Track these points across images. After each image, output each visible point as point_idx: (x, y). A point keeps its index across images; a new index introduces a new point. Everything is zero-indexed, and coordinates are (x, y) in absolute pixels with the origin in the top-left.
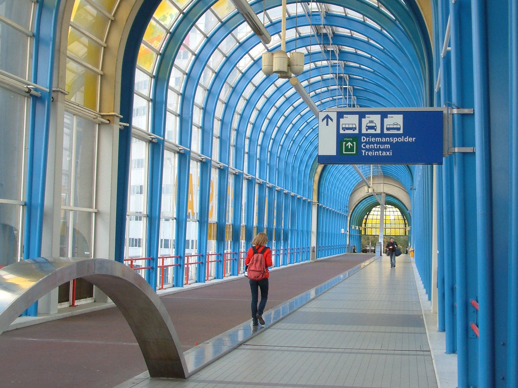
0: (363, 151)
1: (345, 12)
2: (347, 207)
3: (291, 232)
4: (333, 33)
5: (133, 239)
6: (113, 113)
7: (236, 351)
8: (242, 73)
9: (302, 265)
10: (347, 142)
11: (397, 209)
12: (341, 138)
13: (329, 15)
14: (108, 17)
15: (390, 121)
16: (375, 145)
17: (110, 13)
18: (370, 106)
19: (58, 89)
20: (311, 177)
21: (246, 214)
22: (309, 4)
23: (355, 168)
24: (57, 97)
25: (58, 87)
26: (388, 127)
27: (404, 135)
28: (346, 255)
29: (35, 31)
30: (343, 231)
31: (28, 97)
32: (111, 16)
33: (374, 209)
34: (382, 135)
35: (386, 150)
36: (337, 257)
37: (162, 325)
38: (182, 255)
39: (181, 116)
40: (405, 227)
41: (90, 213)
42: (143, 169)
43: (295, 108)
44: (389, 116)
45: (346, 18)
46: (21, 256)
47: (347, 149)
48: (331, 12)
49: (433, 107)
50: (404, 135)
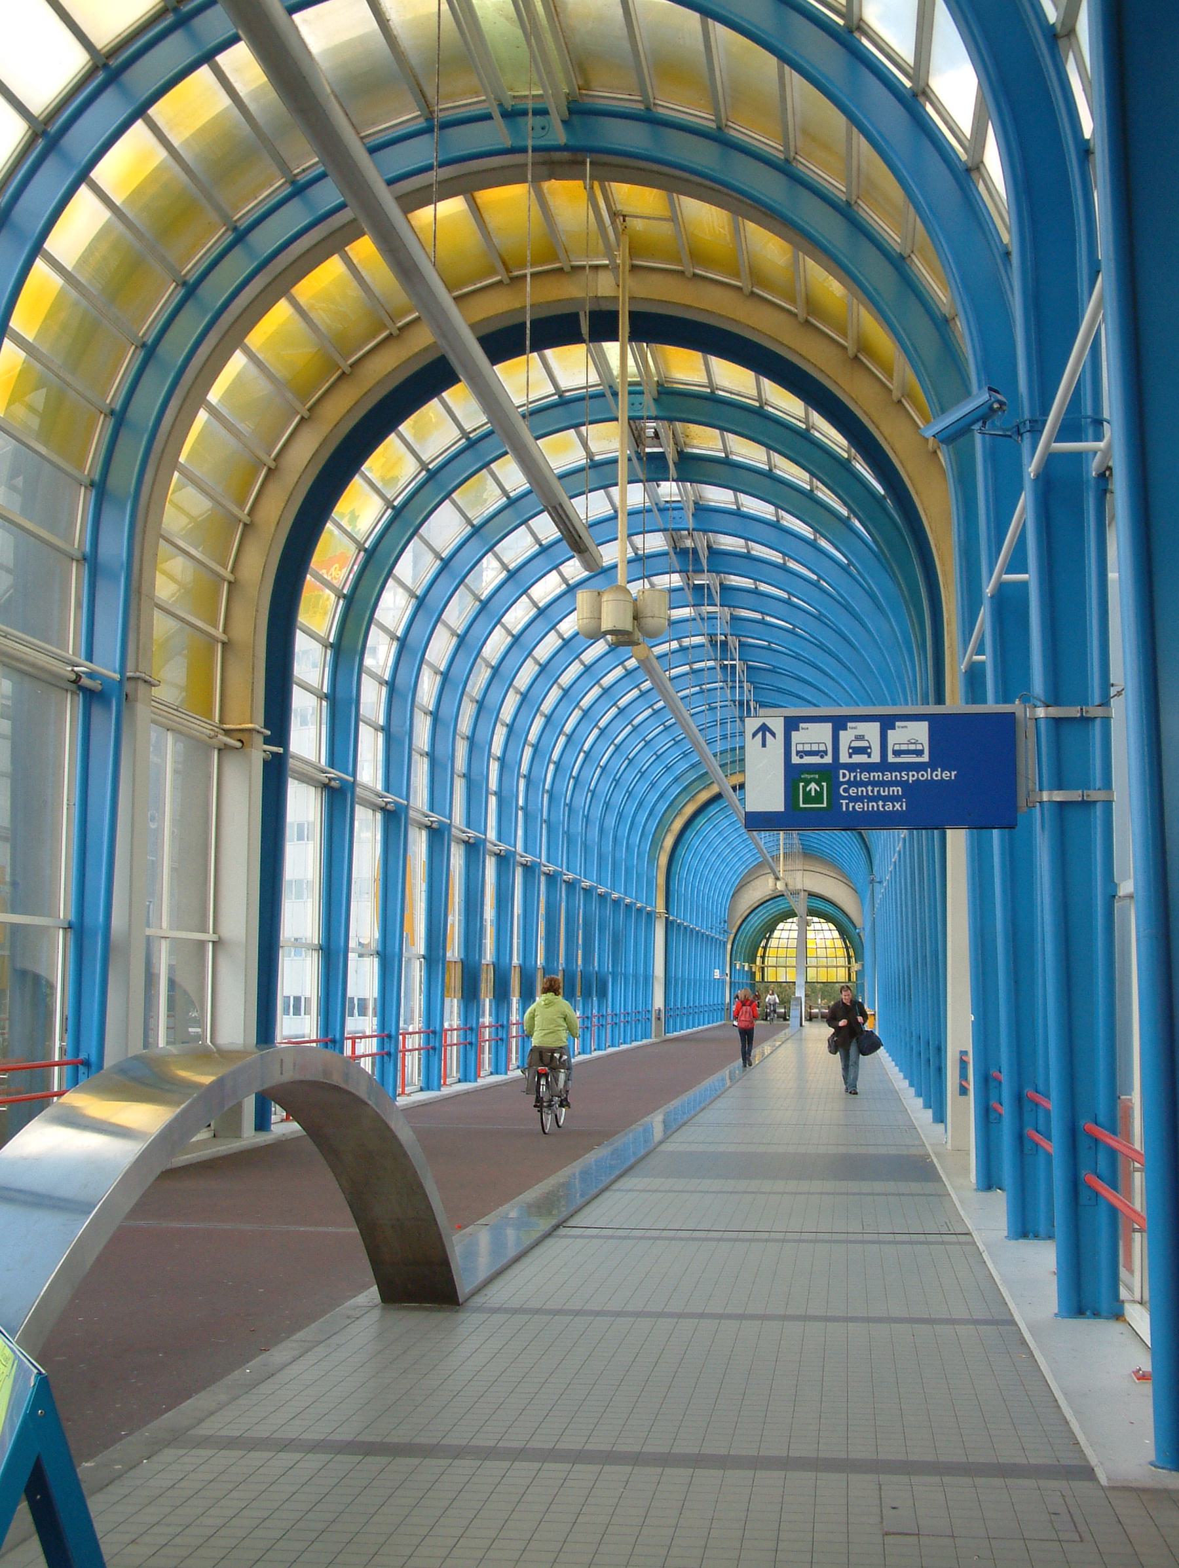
0: (844, 802)
1: (737, 502)
2: (725, 922)
3: (613, 979)
4: (709, 547)
5: (289, 997)
6: (250, 726)
7: (550, 1242)
8: (513, 636)
9: (638, 1048)
10: (808, 782)
11: (830, 924)
12: (793, 775)
13: (702, 510)
14: (235, 516)
15: (901, 736)
16: (870, 788)
17: (241, 506)
18: (782, 704)
19: (138, 674)
20: (653, 859)
21: (521, 941)
22: (658, 486)
23: (753, 838)
24: (136, 690)
25: (137, 670)
26: (897, 748)
27: (933, 765)
28: (724, 1025)
29: (88, 548)
30: (717, 974)
31: (73, 693)
32: (243, 515)
33: (781, 926)
34: (884, 766)
35: (893, 799)
36: (707, 1030)
37: (416, 1189)
38: (393, 1033)
39: (387, 730)
40: (849, 963)
41: (202, 944)
42: (311, 845)
43: (621, 711)
44: (898, 724)
45: (738, 514)
46: (62, 1040)
47: (808, 798)
48: (706, 503)
49: (986, 703)
50: (933, 765)
